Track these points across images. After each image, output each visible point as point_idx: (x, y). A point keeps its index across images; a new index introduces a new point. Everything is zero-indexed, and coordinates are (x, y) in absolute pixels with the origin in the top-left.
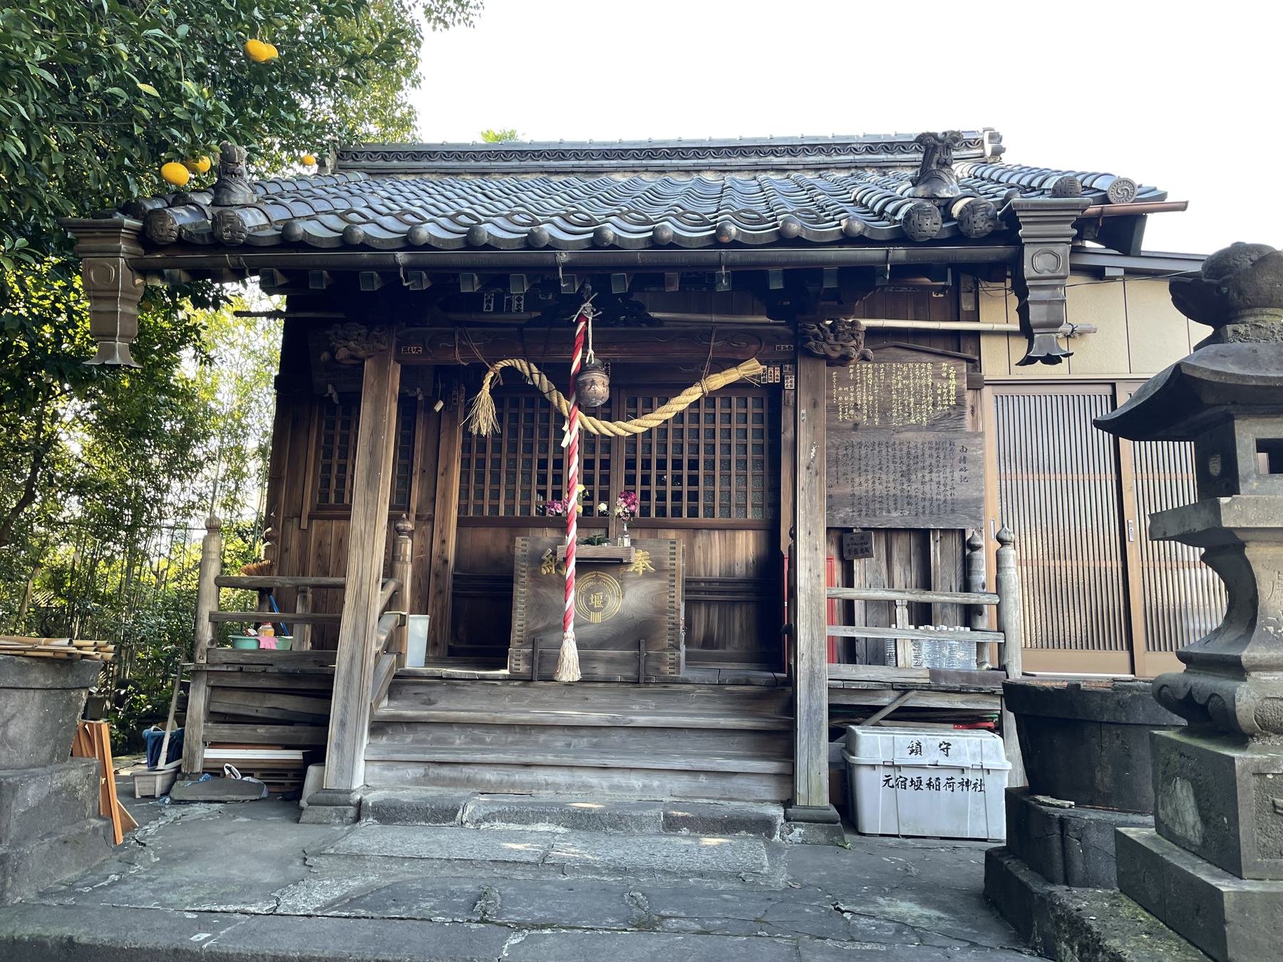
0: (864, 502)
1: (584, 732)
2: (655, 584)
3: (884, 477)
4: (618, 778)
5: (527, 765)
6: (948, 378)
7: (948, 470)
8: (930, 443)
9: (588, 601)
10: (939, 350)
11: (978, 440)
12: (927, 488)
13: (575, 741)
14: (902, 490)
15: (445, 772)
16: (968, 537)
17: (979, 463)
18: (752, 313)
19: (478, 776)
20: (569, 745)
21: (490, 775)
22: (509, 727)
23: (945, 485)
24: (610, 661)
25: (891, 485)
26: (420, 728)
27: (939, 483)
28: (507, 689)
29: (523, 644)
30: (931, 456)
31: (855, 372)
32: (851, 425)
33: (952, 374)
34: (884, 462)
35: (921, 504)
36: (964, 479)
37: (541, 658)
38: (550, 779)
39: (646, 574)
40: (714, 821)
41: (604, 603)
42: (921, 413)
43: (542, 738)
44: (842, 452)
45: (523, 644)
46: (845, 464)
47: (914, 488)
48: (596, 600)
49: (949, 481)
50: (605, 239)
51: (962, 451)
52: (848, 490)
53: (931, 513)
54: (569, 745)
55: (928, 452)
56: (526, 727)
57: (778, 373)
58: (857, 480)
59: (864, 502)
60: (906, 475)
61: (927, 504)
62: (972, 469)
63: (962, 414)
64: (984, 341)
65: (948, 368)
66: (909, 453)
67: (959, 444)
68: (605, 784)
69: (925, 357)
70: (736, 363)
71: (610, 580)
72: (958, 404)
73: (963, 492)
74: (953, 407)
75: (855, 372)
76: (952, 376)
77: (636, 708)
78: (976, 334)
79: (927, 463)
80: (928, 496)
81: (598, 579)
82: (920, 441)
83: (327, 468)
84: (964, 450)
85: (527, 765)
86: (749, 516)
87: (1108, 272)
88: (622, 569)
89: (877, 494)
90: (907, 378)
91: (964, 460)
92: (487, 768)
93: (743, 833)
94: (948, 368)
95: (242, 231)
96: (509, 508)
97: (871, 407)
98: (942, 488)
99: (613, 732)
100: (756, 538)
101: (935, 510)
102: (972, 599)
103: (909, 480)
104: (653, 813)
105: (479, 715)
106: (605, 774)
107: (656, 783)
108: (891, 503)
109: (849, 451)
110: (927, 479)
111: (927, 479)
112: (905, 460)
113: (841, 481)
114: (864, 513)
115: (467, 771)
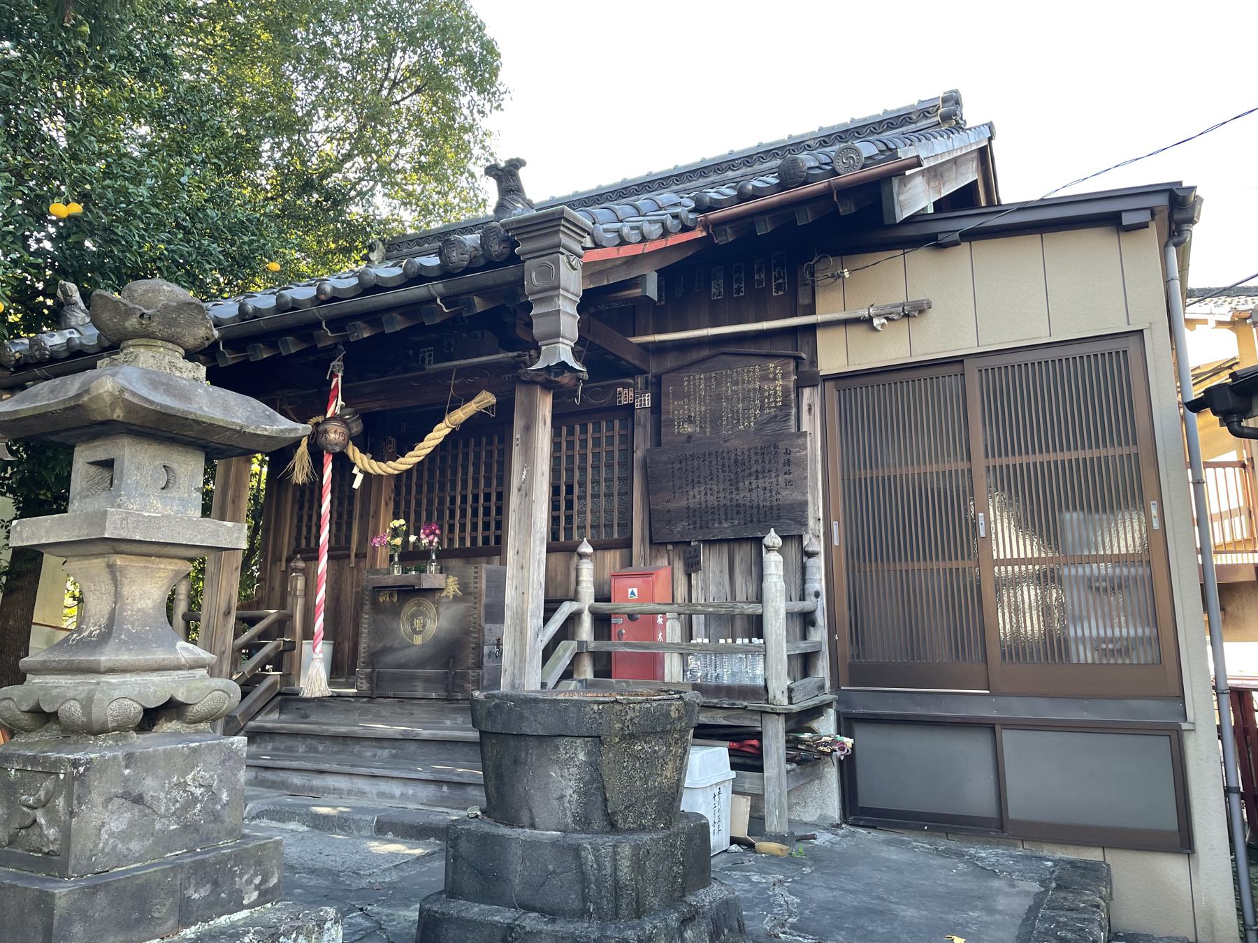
0: (697, 514)
1: (386, 744)
2: (460, 608)
3: (715, 487)
4: (384, 786)
5: (321, 772)
6: (775, 379)
7: (773, 475)
8: (756, 448)
9: (412, 625)
10: (764, 352)
11: (800, 441)
12: (754, 494)
13: (379, 752)
14: (731, 500)
15: (269, 775)
16: (805, 543)
17: (802, 464)
18: (646, 334)
19: (289, 781)
20: (375, 755)
21: (297, 780)
22: (334, 738)
23: (771, 491)
24: (427, 680)
25: (722, 495)
26: (277, 738)
27: (765, 489)
28: (359, 705)
29: (367, 664)
30: (757, 461)
31: (689, 385)
32: (684, 438)
33: (780, 378)
34: (714, 472)
35: (749, 512)
36: (788, 483)
37: (378, 677)
38: (337, 785)
39: (456, 598)
40: (412, 827)
41: (424, 626)
42: (749, 418)
43: (357, 748)
44: (677, 466)
45: (367, 664)
46: (680, 478)
47: (743, 496)
48: (418, 623)
49: (774, 486)
50: (247, 313)
51: (786, 453)
52: (684, 503)
53: (759, 521)
54: (375, 755)
55: (754, 458)
56: (346, 739)
57: (631, 394)
58: (691, 493)
59: (697, 514)
60: (735, 482)
61: (755, 511)
62: (796, 473)
63: (788, 415)
64: (821, 336)
65: (775, 368)
66: (736, 461)
67: (782, 445)
68: (374, 791)
69: (753, 360)
70: (469, 399)
71: (428, 605)
72: (784, 405)
73: (788, 496)
74: (780, 409)
75: (689, 385)
76: (779, 376)
77: (448, 723)
78: (812, 328)
79: (753, 469)
80: (755, 504)
81: (419, 605)
82: (746, 447)
83: (300, 519)
84: (788, 452)
85: (321, 772)
86: (616, 536)
87: (1127, 220)
88: (437, 595)
89: (709, 505)
90: (736, 383)
91: (788, 463)
92: (295, 773)
93: (432, 840)
94: (775, 368)
95: (46, 349)
96: (474, 540)
97: (703, 419)
98: (768, 494)
99: (407, 745)
100: (621, 556)
101: (762, 516)
102: (808, 605)
103: (737, 489)
104: (369, 818)
105: (447, 732)
106: (374, 781)
107: (410, 792)
108: (722, 513)
109: (683, 464)
110: (754, 486)
111: (754, 486)
112: (733, 468)
113: (677, 495)
114: (698, 526)
115: (283, 776)
